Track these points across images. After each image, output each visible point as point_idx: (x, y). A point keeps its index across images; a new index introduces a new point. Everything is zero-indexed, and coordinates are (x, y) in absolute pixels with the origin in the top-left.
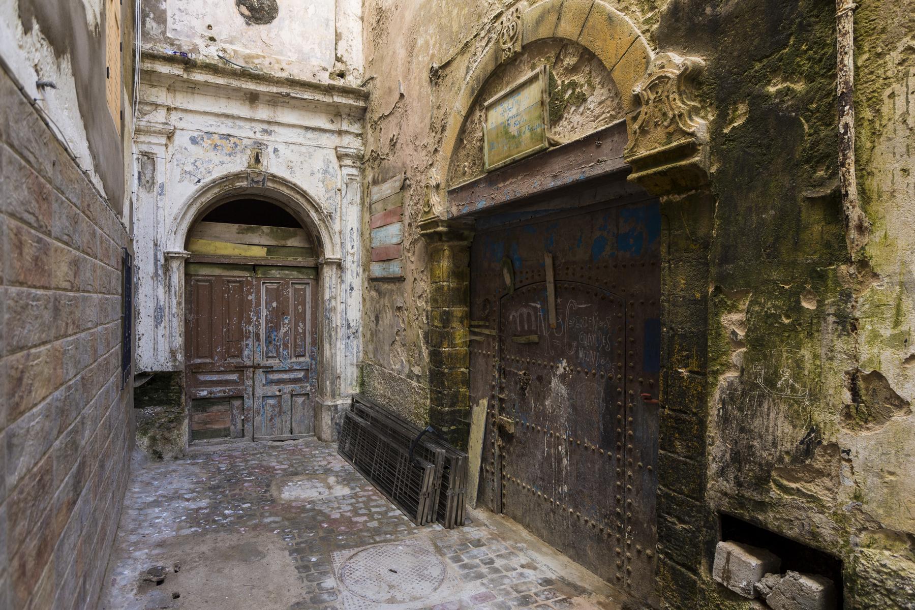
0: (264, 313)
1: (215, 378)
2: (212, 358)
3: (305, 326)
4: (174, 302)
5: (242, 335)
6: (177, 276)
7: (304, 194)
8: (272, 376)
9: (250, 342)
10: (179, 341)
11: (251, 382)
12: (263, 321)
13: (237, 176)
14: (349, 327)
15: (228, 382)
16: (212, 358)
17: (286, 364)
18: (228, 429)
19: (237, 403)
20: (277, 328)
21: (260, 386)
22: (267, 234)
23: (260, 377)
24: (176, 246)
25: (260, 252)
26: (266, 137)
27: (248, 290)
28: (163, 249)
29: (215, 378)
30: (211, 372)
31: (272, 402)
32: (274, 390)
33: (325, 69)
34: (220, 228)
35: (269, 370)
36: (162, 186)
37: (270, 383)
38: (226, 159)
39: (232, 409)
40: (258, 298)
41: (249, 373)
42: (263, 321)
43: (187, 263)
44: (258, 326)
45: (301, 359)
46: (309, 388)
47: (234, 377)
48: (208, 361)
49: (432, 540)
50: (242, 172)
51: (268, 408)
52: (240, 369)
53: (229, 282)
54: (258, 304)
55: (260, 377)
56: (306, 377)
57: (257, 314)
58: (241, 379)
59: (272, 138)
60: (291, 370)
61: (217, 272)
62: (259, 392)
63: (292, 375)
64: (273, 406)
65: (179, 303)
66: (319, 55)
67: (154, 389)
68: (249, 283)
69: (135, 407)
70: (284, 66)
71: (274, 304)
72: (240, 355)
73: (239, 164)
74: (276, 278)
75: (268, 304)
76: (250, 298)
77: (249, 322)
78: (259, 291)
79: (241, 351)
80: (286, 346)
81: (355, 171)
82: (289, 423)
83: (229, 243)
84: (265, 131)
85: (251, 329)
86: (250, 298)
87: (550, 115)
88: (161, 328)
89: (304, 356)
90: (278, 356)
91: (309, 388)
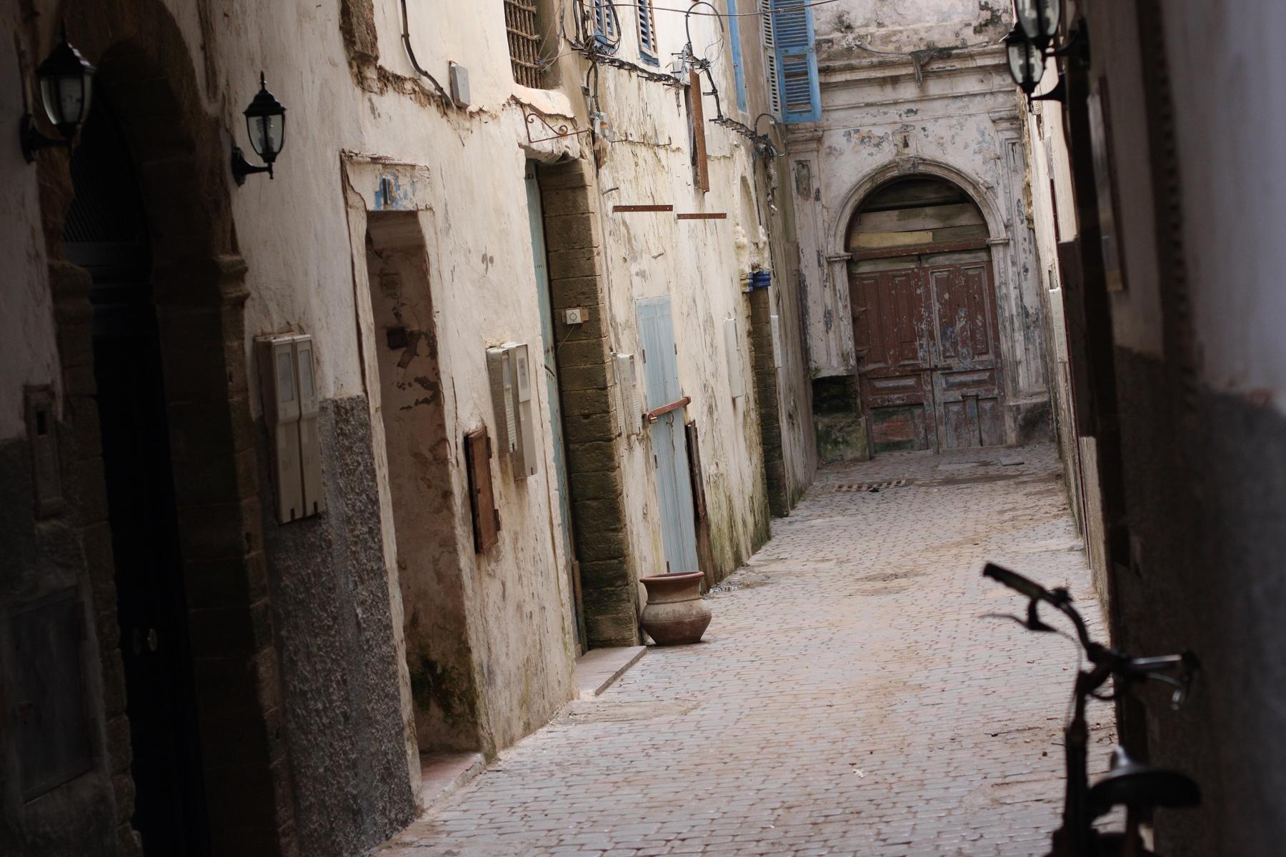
0: (936, 307)
1: (891, 384)
2: (886, 362)
3: (984, 317)
4: (840, 305)
5: (915, 335)
6: (841, 274)
7: (958, 173)
8: (952, 379)
9: (924, 341)
10: (849, 345)
11: (929, 387)
12: (936, 316)
13: (885, 168)
14: (1027, 315)
15: (905, 388)
16: (886, 362)
17: (968, 364)
18: (910, 441)
19: (918, 411)
20: (952, 323)
21: (940, 392)
22: (931, 217)
23: (940, 381)
24: (836, 247)
25: (926, 238)
26: (912, 118)
27: (916, 284)
28: (825, 254)
29: (891, 384)
30: (887, 378)
31: (955, 408)
32: (956, 395)
33: (968, 25)
34: (888, 218)
35: (948, 371)
36: (818, 191)
37: (951, 386)
38: (874, 150)
39: (913, 418)
40: (928, 292)
41: (925, 377)
42: (936, 316)
43: (850, 263)
44: (930, 323)
45: (984, 357)
46: (996, 392)
47: (910, 382)
48: (881, 365)
49: (447, 233)
50: (891, 163)
51: (951, 415)
52: (916, 372)
53: (895, 276)
54: (928, 297)
55: (940, 381)
56: (991, 377)
57: (929, 308)
58: (919, 383)
59: (918, 117)
60: (973, 371)
61: (883, 266)
62: (939, 397)
63: (976, 377)
64: (957, 413)
65: (845, 307)
66: (960, 9)
67: (828, 396)
68: (917, 276)
69: (815, 413)
70: (923, 35)
71: (947, 296)
72: (915, 357)
73: (885, 155)
74: (945, 266)
75: (940, 296)
76: (918, 292)
77: (920, 320)
78: (928, 282)
79: (915, 352)
80: (964, 344)
81: (1010, 134)
82: (977, 433)
83: (892, 232)
84: (910, 111)
85: (923, 326)
86: (918, 292)
87: (395, 673)
88: (831, 333)
89: (987, 353)
90: (957, 355)
91: (996, 392)
